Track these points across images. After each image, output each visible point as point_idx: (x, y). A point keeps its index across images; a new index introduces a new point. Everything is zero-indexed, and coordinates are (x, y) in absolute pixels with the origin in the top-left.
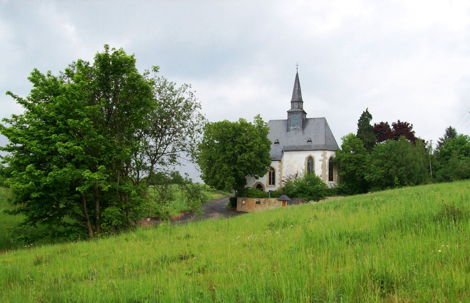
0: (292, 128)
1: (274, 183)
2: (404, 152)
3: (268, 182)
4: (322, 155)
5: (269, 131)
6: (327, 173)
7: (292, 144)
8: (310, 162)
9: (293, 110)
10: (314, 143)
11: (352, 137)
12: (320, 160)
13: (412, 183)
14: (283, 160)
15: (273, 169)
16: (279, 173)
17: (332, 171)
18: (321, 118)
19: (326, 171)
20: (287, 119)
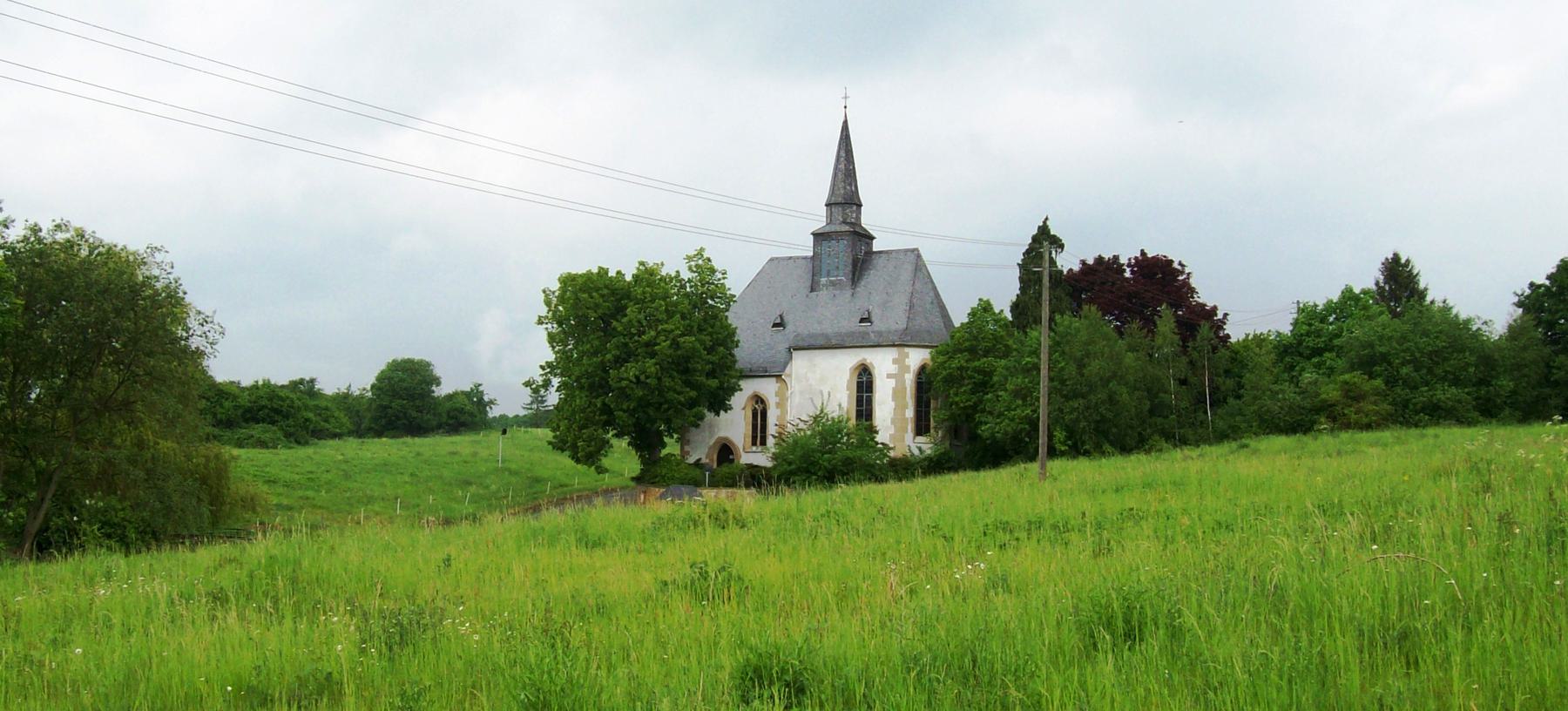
0: (823, 280)
1: (763, 443)
2: (1088, 355)
3: (750, 440)
4: (895, 361)
6: (910, 413)
7: (816, 328)
8: (864, 383)
9: (828, 229)
10: (879, 324)
12: (889, 376)
13: (1107, 447)
14: (790, 376)
16: (778, 412)
17: (928, 405)
18: (906, 251)
19: (905, 407)
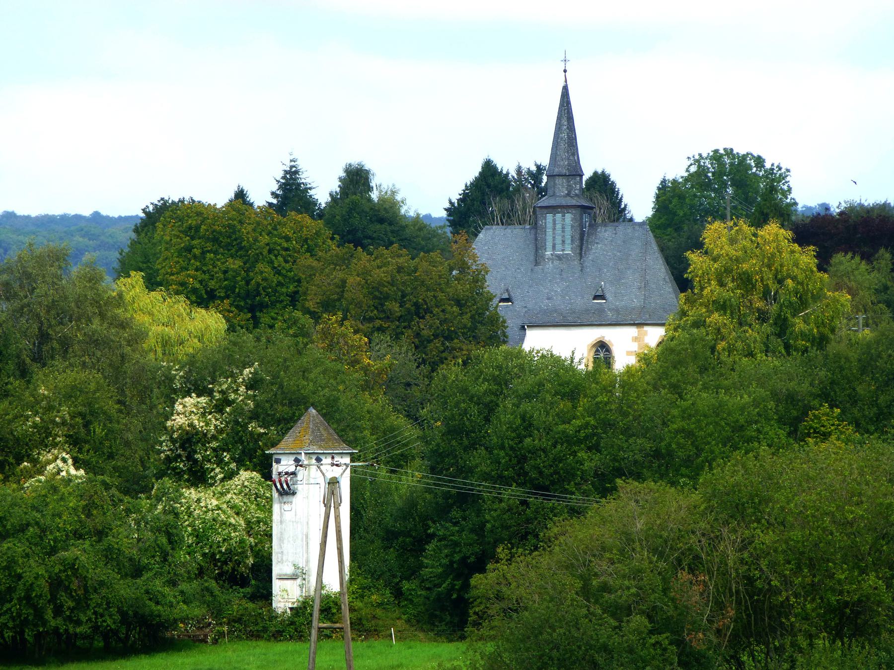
5: (399, 198)
7: (545, 304)
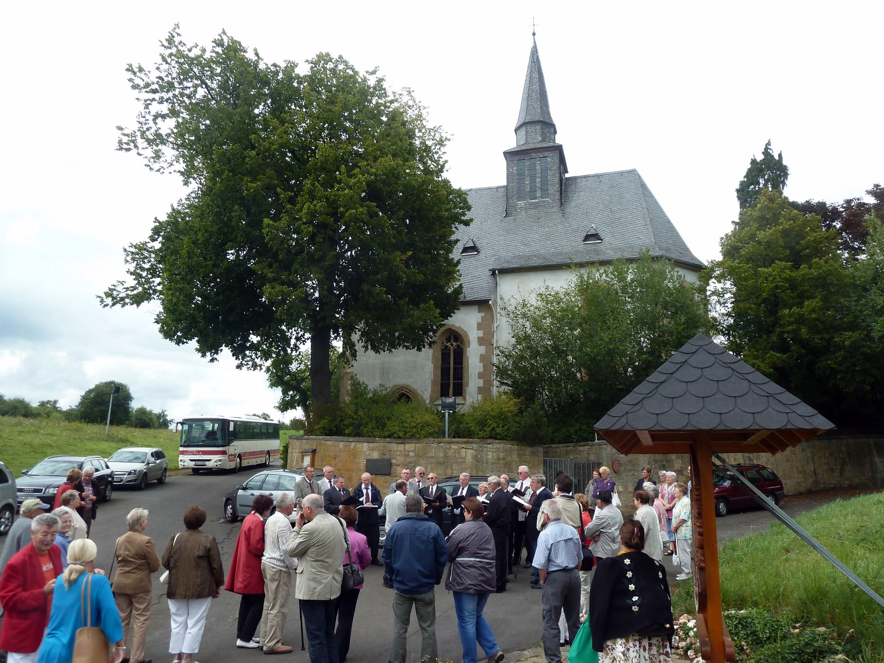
1: (459, 391)
11: (650, 288)
15: (456, 337)
16: (482, 350)
20: (505, 183)
